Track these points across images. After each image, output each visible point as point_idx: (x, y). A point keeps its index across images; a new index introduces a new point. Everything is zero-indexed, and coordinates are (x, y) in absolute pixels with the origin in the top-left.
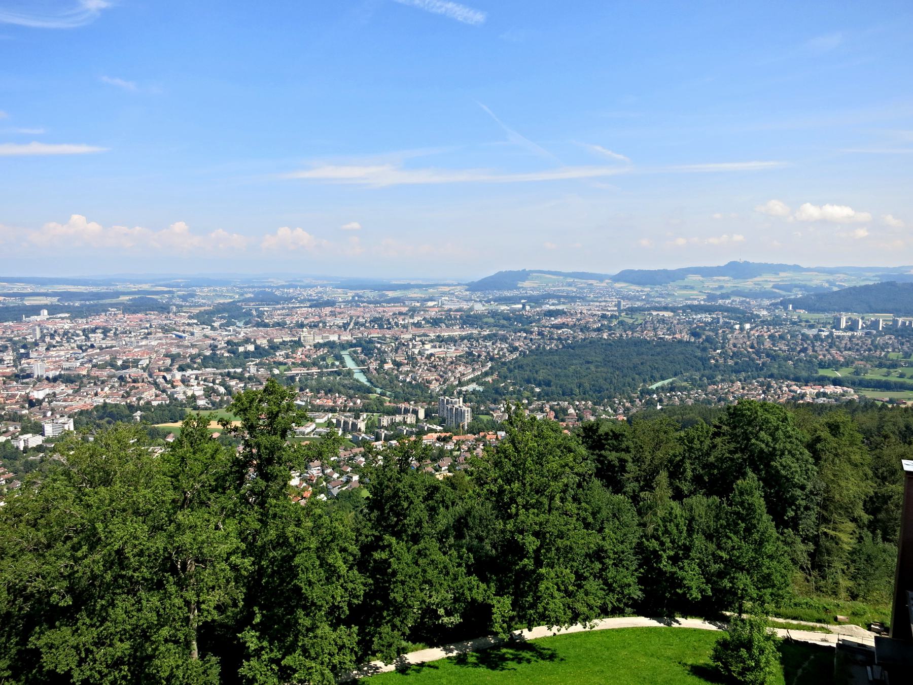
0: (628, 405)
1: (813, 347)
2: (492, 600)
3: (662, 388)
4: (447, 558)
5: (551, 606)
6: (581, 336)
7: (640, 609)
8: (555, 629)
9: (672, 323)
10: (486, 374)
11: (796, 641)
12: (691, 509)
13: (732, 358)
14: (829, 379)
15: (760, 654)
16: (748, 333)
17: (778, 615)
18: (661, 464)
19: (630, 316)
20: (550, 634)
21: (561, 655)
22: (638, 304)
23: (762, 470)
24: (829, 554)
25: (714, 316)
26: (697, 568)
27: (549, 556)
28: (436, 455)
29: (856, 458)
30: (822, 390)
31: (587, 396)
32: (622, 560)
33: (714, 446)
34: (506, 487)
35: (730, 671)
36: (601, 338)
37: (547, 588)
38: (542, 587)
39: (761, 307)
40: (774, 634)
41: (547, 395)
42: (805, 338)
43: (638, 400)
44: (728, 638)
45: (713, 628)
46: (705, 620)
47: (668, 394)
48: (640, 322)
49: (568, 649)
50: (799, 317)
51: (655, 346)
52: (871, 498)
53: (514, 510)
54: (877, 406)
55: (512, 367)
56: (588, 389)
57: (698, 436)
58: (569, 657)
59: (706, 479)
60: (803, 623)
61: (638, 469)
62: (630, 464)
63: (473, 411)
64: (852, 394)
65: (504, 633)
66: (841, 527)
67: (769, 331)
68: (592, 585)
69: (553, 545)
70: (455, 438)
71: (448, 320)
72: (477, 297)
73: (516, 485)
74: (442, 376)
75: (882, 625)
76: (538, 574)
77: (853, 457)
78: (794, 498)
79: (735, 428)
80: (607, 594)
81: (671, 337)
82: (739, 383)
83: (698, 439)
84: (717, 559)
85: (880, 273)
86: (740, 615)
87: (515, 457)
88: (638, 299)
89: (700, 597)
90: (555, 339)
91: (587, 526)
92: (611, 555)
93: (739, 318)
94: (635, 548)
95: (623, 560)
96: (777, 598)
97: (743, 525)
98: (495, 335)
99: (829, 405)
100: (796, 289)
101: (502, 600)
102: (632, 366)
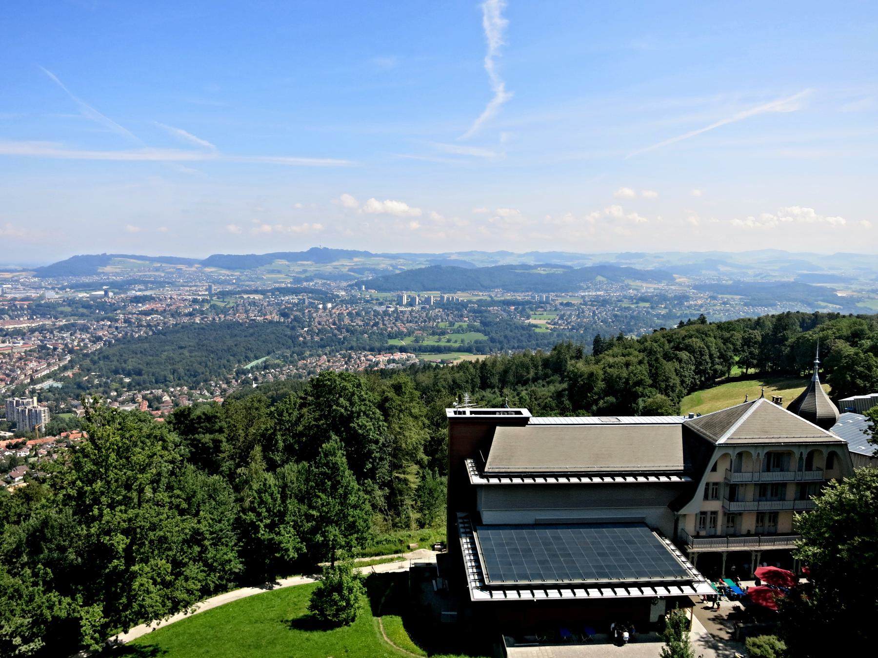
0: (224, 386)
1: (383, 321)
2: (78, 612)
3: (257, 367)
4: (18, 581)
5: (148, 601)
6: (172, 321)
7: (242, 581)
8: (154, 624)
9: (262, 305)
10: (65, 368)
11: (380, 574)
12: (284, 477)
13: (318, 334)
14: (396, 347)
15: (349, 594)
16: (330, 312)
17: (364, 555)
18: (254, 439)
19: (221, 300)
20: (149, 630)
21: (164, 648)
22: (229, 288)
23: (343, 432)
24: (401, 495)
25: (300, 297)
26: (292, 530)
27: (142, 550)
28: (7, 466)
29: (416, 411)
30: (391, 357)
31: (182, 381)
32: (220, 539)
33: (302, 416)
34: (86, 488)
35: (326, 616)
36: (193, 323)
37: (142, 585)
38: (136, 585)
39: (339, 288)
40: (359, 573)
41: (139, 384)
42: (376, 313)
43: (234, 381)
44: (323, 587)
45: (310, 581)
46: (303, 576)
47: (263, 372)
48: (232, 305)
49: (171, 640)
50: (371, 296)
51: (247, 328)
52: (430, 442)
53: (96, 512)
54: (432, 366)
55: (96, 358)
56: (183, 374)
57: (287, 409)
58: (172, 648)
59: (296, 447)
60: (384, 557)
61: (232, 447)
62: (225, 444)
63: (51, 410)
64: (414, 359)
65: (97, 643)
66: (408, 470)
67: (347, 309)
68: (193, 570)
69: (146, 539)
70: (30, 444)
71: (13, 311)
72: (49, 284)
73: (99, 485)
74: (8, 375)
75: (442, 544)
76: (131, 572)
77: (413, 411)
78: (371, 452)
79: (317, 398)
80: (209, 575)
81: (262, 318)
82: (325, 357)
83: (287, 412)
84: (309, 518)
85: (429, 259)
86: (333, 565)
87: (95, 455)
88: (228, 282)
89: (296, 556)
90: (144, 326)
91: (182, 512)
92: (207, 536)
93: (322, 298)
94: (233, 524)
95: (222, 538)
96: (361, 541)
97: (329, 483)
98: (73, 325)
99: (500, 368)
100: (367, 272)
101: (91, 610)
102: (225, 348)
